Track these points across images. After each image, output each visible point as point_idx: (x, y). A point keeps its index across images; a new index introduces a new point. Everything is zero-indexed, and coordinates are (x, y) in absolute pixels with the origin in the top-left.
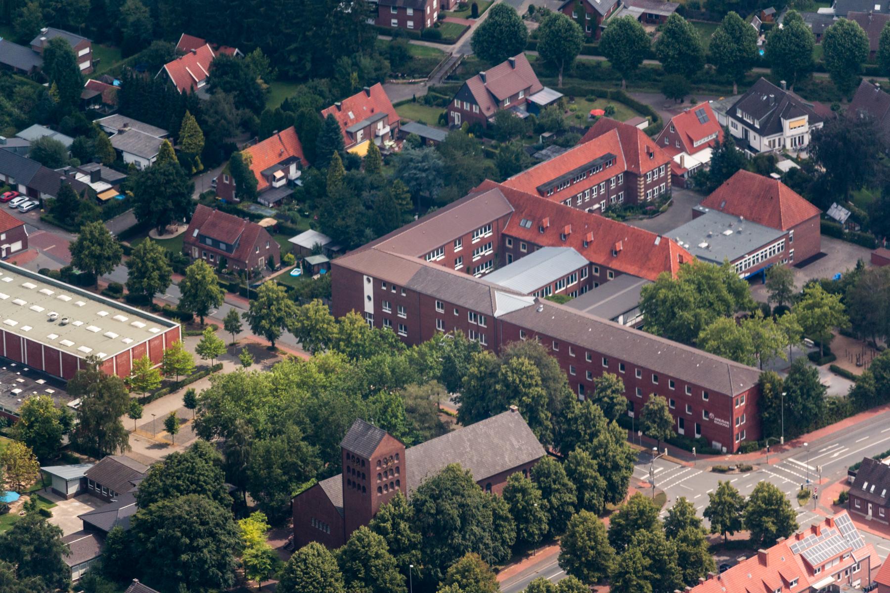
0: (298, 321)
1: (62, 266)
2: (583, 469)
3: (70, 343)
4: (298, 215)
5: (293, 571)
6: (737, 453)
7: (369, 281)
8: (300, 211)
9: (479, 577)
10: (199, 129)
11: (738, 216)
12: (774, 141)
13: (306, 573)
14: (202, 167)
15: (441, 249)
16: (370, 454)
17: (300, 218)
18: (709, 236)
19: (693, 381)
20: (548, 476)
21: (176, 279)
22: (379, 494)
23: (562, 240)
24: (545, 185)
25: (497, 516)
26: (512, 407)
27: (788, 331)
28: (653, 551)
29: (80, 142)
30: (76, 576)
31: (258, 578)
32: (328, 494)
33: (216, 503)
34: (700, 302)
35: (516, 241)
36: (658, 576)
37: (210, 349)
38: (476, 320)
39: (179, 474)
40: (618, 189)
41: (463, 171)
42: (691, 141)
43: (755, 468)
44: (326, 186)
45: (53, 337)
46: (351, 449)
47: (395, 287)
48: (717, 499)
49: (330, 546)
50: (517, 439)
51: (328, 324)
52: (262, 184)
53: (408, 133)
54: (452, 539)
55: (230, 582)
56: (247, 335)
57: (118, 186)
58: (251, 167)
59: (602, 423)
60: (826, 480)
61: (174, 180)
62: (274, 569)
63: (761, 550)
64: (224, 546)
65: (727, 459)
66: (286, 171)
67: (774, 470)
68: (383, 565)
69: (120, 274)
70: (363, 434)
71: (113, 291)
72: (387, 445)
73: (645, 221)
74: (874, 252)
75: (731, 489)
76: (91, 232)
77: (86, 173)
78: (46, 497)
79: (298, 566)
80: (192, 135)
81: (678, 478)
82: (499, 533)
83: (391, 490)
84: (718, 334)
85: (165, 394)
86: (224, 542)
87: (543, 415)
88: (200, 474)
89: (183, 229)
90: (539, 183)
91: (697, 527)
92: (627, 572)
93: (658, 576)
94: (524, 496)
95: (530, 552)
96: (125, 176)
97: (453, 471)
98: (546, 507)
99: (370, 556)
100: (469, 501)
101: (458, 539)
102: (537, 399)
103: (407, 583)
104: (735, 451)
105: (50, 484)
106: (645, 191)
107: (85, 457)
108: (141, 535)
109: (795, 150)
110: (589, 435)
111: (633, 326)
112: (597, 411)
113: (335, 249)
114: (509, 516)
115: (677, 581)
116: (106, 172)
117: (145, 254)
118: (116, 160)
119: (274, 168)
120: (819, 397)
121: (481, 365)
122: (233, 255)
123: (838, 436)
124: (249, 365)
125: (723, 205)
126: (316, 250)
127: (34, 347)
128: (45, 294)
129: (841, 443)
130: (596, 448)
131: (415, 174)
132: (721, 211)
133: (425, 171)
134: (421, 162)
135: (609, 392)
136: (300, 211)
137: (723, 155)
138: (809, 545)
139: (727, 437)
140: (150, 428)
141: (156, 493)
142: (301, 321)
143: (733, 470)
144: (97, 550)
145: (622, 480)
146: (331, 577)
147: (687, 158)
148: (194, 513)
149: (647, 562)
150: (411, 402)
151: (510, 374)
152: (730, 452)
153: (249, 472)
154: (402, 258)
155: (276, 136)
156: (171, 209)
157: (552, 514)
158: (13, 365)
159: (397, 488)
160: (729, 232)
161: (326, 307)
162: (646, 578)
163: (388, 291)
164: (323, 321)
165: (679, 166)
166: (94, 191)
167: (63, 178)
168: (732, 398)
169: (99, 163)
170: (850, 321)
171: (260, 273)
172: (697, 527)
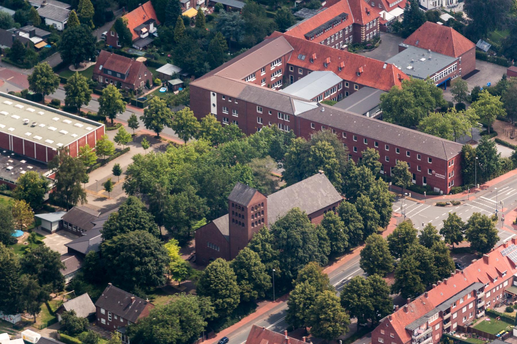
0: (175, 120)
1: (21, 90)
2: (367, 208)
3: (40, 138)
4: (158, 55)
5: (209, 276)
6: (449, 194)
7: (214, 95)
8: (158, 52)
9: (319, 276)
10: (91, 4)
11: (427, 49)
12: (436, 2)
13: (217, 277)
14: (94, 26)
15: (254, 74)
16: (248, 203)
17: (159, 56)
18: (412, 62)
19: (422, 152)
20: (347, 212)
21: (95, 97)
22: (252, 227)
23: (324, 67)
24: (309, 33)
25: (320, 238)
26: (320, 171)
27: (471, 119)
28: (421, 257)
29: (20, 13)
30: (67, 281)
31: (179, 280)
32: (219, 228)
33: (151, 234)
34: (417, 103)
35: (296, 68)
36: (424, 272)
37: (123, 139)
38: (283, 117)
39: (128, 218)
40: (350, 34)
41: (257, 26)
42: (388, 4)
43: (462, 203)
44: (173, 36)
45: (29, 134)
46: (235, 201)
47: (231, 98)
48: (449, 224)
49: (228, 259)
50: (324, 190)
51: (194, 122)
52: (135, 36)
53: (216, 3)
54: (297, 254)
55: (164, 282)
56: (142, 129)
57: (46, 39)
58: (128, 26)
59: (372, 178)
60: (506, 209)
61: (85, 36)
62: (189, 274)
63: (484, 255)
64: (160, 261)
65: (444, 198)
66: (148, 28)
67: (473, 204)
68: (259, 270)
69: (60, 94)
70: (242, 192)
71: (55, 104)
72: (257, 198)
73: (367, 53)
74: (509, 69)
75: (457, 217)
76: (41, 69)
77: (25, 32)
78: (39, 233)
79: (212, 274)
80: (87, 7)
81: (417, 210)
82: (321, 248)
83: (259, 225)
84: (432, 123)
85: (98, 167)
86: (160, 259)
87: (337, 176)
88: (141, 218)
89: (90, 64)
90: (305, 32)
91: (438, 241)
92: (407, 271)
93: (424, 272)
94: (334, 226)
95: (337, 258)
96: (49, 33)
97: (296, 212)
98: (346, 230)
99: (251, 265)
100: (307, 230)
101: (301, 253)
102: (334, 165)
103: (272, 280)
104: (448, 193)
105: (41, 224)
106: (365, 35)
107: (57, 207)
108: (110, 256)
109: (449, 8)
110: (365, 186)
111: (374, 118)
112: (371, 172)
113: (185, 75)
114: (327, 237)
115: (435, 275)
116: (38, 31)
117: (76, 82)
118: (41, 23)
119: (141, 27)
120: (496, 159)
121: (297, 146)
122: (125, 80)
123: (507, 182)
124: (147, 148)
125: (417, 43)
126: (174, 77)
127: (18, 141)
128: (18, 108)
129: (510, 186)
130: (373, 194)
131: (229, 28)
132: (416, 46)
133: (233, 26)
134: (231, 21)
135: (371, 160)
136: (158, 52)
137: (411, 12)
138: (511, 250)
139: (443, 185)
140: (94, 188)
141: (116, 230)
142: (178, 121)
143: (449, 204)
144: (79, 265)
145: (388, 213)
146: (231, 279)
147: (387, 14)
148: (142, 242)
149: (418, 263)
150: (256, 170)
151: (317, 151)
152: (445, 193)
153: (165, 215)
154: (233, 79)
155: (141, 7)
156: (84, 54)
157: (350, 235)
158: (4, 152)
159: (262, 223)
160: (423, 59)
161: (192, 112)
162: (416, 273)
163: (226, 101)
164: (191, 121)
165: (382, 19)
166: (33, 43)
167: (14, 35)
168: (447, 161)
169: (31, 25)
170: (506, 111)
171: (141, 91)
172: (438, 241)
